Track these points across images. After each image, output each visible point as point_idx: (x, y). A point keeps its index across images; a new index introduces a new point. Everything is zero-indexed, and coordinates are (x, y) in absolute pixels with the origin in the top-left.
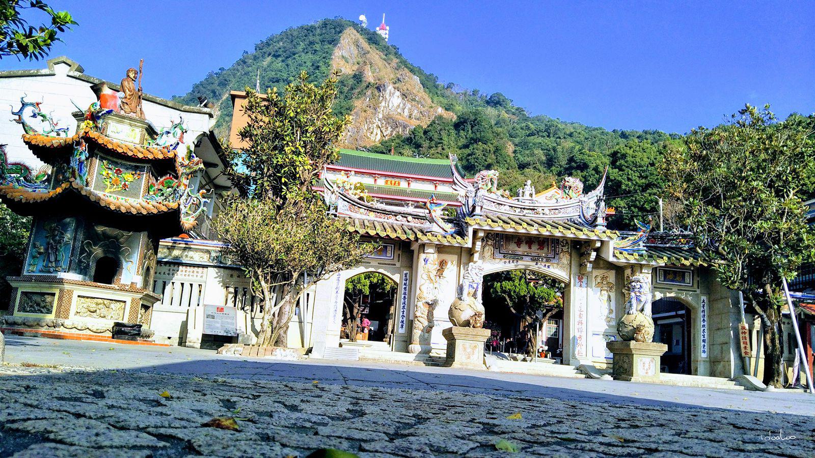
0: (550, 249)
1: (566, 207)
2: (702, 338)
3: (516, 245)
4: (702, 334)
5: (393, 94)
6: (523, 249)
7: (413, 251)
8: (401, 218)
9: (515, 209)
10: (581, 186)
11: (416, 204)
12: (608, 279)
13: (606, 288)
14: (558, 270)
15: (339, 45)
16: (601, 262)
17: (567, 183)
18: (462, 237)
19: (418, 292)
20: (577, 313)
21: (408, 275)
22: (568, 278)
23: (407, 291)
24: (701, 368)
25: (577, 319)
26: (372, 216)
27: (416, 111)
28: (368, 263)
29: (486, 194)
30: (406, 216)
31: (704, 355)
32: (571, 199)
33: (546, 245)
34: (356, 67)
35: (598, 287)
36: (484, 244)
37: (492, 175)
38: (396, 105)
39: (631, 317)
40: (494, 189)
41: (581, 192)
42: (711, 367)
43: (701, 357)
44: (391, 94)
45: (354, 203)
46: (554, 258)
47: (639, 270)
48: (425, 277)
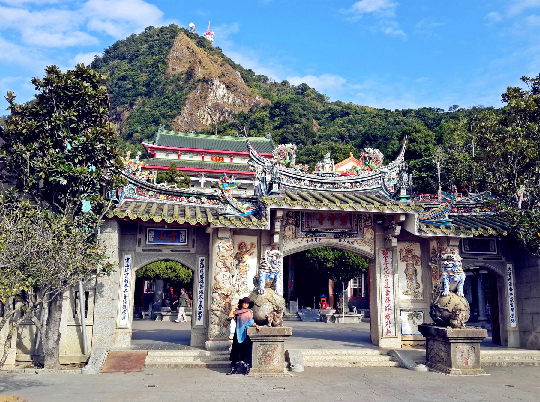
0: (353, 224)
1: (366, 180)
2: (510, 308)
3: (318, 222)
4: (510, 303)
5: (220, 86)
6: (327, 225)
7: (209, 234)
8: (195, 199)
9: (316, 184)
10: (381, 156)
11: (238, 176)
12: (413, 252)
13: (412, 262)
14: (363, 244)
15: (173, 47)
16: (406, 236)
17: (367, 155)
18: (258, 218)
19: (213, 282)
20: (384, 290)
21: (204, 261)
22: (372, 252)
23: (204, 279)
24: (512, 339)
25: (384, 296)
26: (162, 198)
27: (238, 100)
28: (159, 250)
29: (285, 169)
30: (200, 196)
31: (513, 325)
32: (372, 170)
33: (351, 222)
34: (187, 66)
35: (403, 261)
36: (284, 223)
37: (289, 149)
38: (221, 94)
39: (445, 300)
40: (293, 164)
41: (381, 163)
42: (521, 337)
43: (511, 327)
44: (218, 87)
45: (142, 186)
46: (358, 233)
47: (446, 243)
48: (220, 264)
